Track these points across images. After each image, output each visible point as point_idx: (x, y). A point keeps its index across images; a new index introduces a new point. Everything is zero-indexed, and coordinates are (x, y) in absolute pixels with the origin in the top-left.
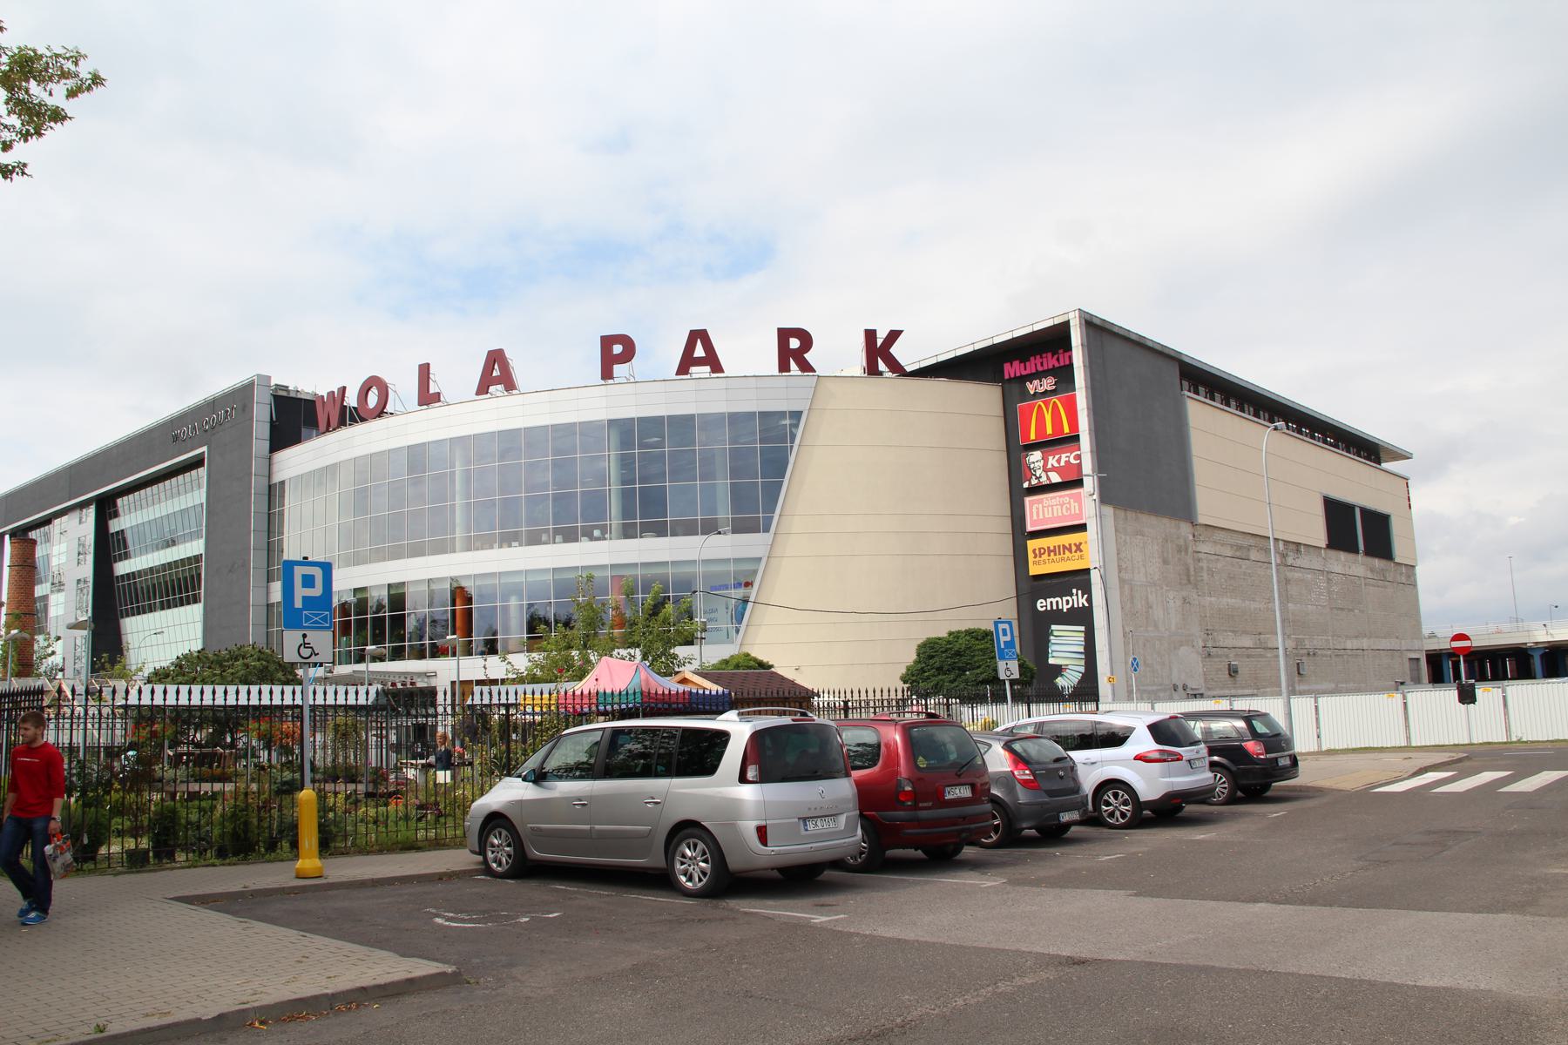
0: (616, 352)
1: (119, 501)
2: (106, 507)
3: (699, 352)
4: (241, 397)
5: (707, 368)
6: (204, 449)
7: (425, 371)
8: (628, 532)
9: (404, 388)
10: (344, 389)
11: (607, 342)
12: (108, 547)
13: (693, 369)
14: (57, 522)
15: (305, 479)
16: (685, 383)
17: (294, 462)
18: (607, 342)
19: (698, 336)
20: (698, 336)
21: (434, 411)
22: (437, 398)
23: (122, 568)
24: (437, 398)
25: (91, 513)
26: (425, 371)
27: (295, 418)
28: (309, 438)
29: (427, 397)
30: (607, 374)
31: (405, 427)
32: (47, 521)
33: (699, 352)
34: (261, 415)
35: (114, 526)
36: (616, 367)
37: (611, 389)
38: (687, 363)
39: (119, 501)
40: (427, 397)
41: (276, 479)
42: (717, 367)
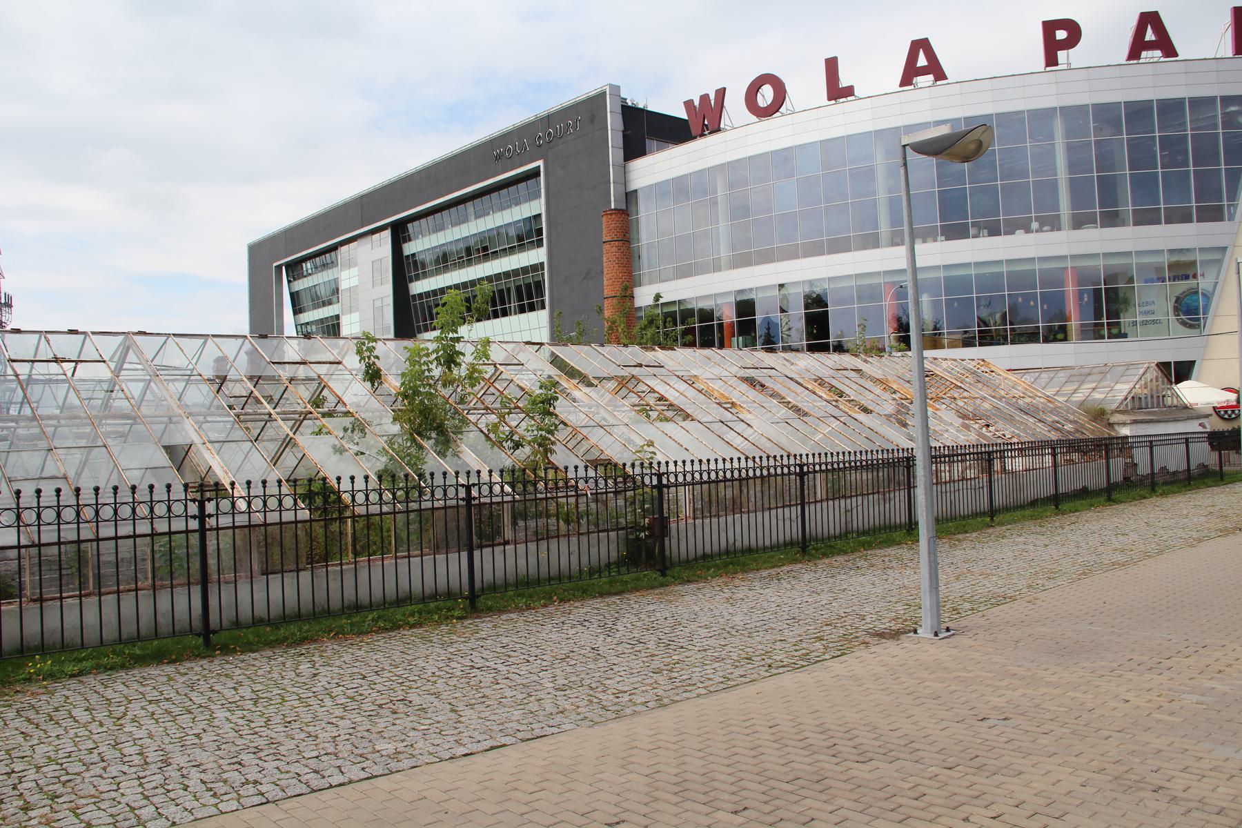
0: (1060, 36)
1: (409, 225)
2: (400, 233)
3: (1151, 35)
4: (592, 106)
5: (931, 77)
6: (540, 163)
7: (832, 66)
8: (1146, 218)
9: (806, 88)
10: (721, 93)
11: (1050, 27)
12: (404, 269)
13: (1144, 54)
14: (344, 249)
15: (660, 189)
16: (1135, 68)
17: (657, 167)
18: (1050, 27)
19: (921, 45)
20: (921, 45)
21: (845, 105)
22: (849, 91)
23: (418, 287)
24: (849, 91)
25: (387, 235)
26: (832, 66)
27: (647, 130)
28: (651, 152)
29: (837, 92)
30: (1051, 60)
31: (741, 138)
32: (334, 248)
33: (922, 61)
34: (613, 123)
35: (409, 249)
36: (1062, 55)
37: (1052, 75)
38: (910, 74)
39: (409, 225)
40: (837, 92)
41: (632, 187)
42: (940, 75)
